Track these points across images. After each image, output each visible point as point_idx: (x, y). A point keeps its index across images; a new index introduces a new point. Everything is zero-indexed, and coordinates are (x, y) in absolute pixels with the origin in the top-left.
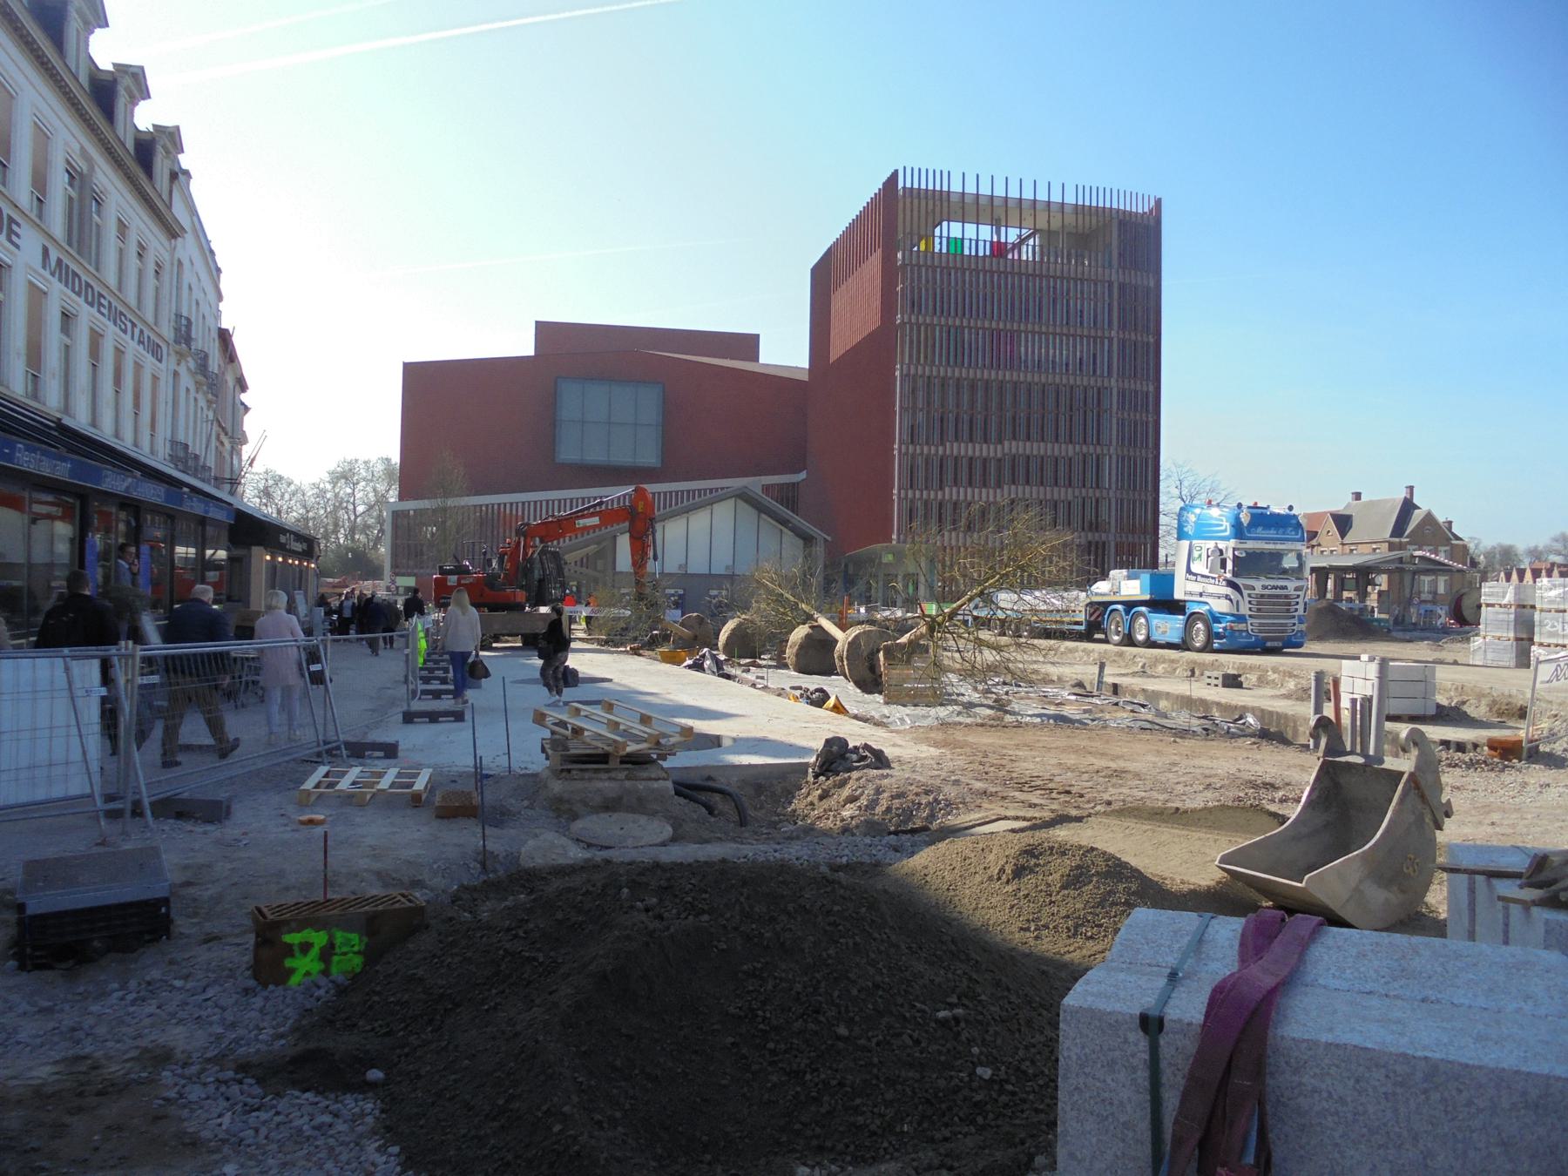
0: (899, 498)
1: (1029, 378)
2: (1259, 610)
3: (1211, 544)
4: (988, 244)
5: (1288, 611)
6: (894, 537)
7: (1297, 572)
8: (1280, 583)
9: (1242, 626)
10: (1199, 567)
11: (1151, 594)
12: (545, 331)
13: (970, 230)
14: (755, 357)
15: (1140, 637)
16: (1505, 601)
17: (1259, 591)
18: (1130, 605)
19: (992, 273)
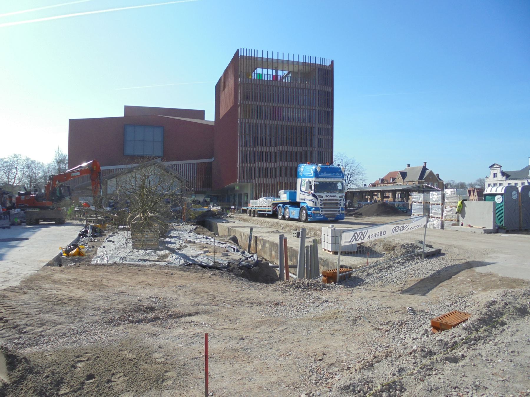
0: (239, 166)
1: (306, 125)
2: (324, 205)
3: (307, 180)
4: (271, 76)
5: (337, 205)
6: (238, 180)
7: (341, 191)
8: (333, 195)
9: (318, 212)
10: (304, 189)
11: (290, 200)
12: (127, 109)
13: (265, 71)
14: (203, 117)
15: (287, 217)
16: (420, 201)
17: (324, 198)
18: (284, 204)
19: (310, 90)
